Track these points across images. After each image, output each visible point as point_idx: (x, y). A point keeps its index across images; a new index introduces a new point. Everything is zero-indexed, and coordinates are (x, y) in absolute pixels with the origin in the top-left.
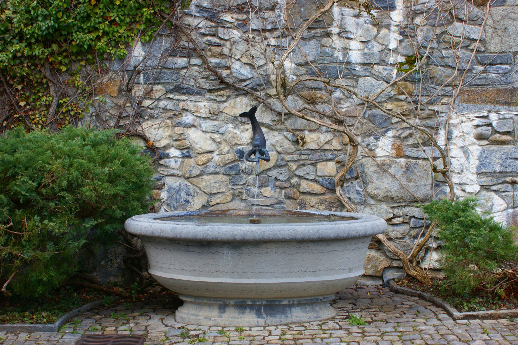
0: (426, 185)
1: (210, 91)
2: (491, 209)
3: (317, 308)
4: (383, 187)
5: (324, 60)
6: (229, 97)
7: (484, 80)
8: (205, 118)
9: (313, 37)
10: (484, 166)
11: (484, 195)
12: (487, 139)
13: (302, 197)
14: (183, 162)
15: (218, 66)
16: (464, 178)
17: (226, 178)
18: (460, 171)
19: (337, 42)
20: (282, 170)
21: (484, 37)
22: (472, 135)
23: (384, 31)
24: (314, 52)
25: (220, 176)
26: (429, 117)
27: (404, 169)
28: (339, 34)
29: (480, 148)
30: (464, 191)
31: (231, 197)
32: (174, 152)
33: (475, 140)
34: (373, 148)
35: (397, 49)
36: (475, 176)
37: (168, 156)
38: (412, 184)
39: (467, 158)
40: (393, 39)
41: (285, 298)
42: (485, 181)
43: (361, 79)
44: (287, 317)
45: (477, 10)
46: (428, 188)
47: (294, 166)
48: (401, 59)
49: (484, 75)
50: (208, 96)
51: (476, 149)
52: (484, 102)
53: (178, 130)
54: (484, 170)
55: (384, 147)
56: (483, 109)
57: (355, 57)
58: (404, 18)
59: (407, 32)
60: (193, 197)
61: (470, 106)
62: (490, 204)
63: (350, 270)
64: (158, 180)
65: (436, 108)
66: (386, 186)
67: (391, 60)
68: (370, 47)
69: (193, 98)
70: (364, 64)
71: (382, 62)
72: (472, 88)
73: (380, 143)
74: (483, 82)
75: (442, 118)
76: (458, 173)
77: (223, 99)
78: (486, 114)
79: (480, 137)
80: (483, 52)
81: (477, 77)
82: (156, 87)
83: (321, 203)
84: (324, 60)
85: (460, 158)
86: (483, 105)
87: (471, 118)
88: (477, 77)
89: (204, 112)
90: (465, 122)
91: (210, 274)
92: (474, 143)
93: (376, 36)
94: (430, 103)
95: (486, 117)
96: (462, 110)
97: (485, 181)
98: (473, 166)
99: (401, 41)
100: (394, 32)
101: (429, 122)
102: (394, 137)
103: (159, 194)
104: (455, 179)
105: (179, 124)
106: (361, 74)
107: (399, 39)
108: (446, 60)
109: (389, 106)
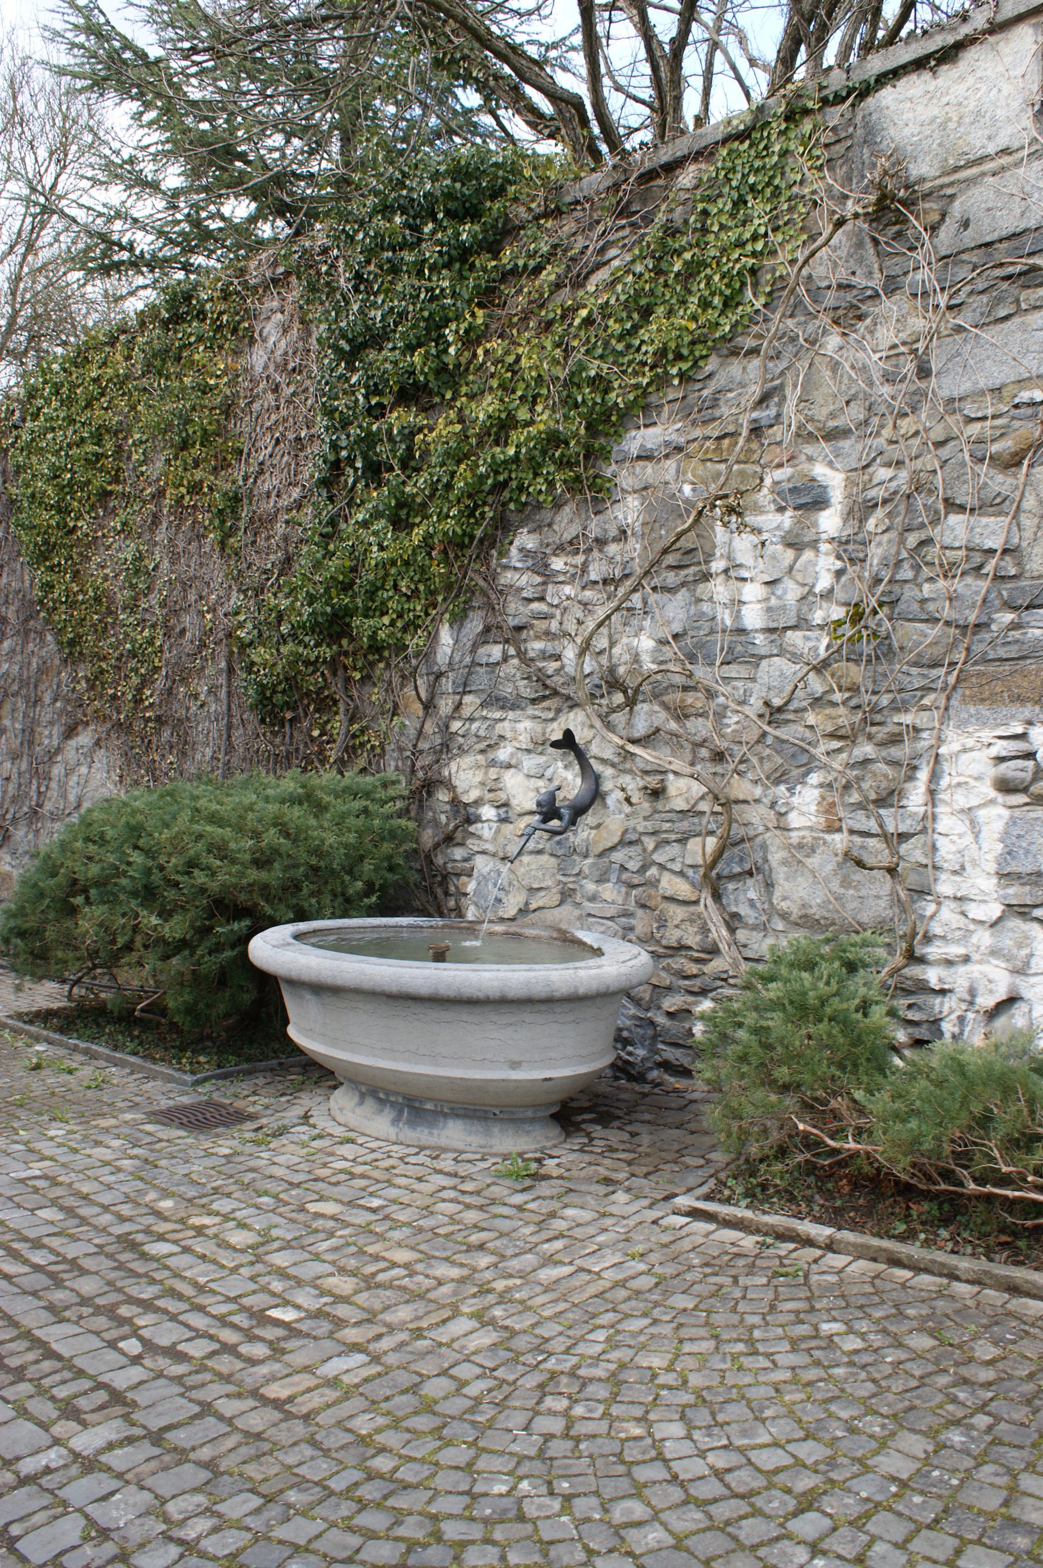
0: (878, 897)
1: (534, 701)
2: (1027, 964)
3: (496, 1130)
4: (795, 896)
5: (698, 628)
6: (558, 711)
7: (1016, 647)
8: (528, 751)
9: (683, 584)
10: (1013, 858)
11: (1012, 930)
12: (1025, 790)
13: (665, 905)
14: (498, 831)
15: (545, 656)
16: (964, 885)
17: (553, 861)
18: (957, 867)
19: (719, 589)
20: (633, 851)
21: (1016, 540)
22: (988, 782)
23: (808, 555)
24: (682, 615)
25: (545, 858)
26: (895, 739)
27: (840, 859)
28: (726, 571)
29: (1006, 813)
30: (964, 914)
31: (558, 897)
32: (488, 812)
33: (993, 793)
34: (783, 810)
35: (831, 591)
36: (994, 880)
37: (478, 819)
38: (851, 892)
39: (977, 836)
40: (823, 568)
41: (429, 1099)
42: (1016, 893)
43: (764, 663)
44: (431, 1134)
45: (1000, 478)
46: (883, 903)
47: (650, 843)
48: (838, 613)
49: (1016, 634)
50: (530, 711)
51: (996, 816)
52: (1019, 699)
53: (493, 773)
54: (1013, 867)
55: (805, 805)
56: (1013, 717)
57: (753, 617)
58: (845, 521)
59: (850, 549)
60: (507, 892)
61: (984, 710)
62: (1024, 952)
63: (515, 1065)
64: (466, 860)
65: (907, 719)
66: (803, 893)
67: (818, 617)
68: (779, 593)
69: (511, 715)
70: (771, 630)
71: (801, 624)
72: (991, 668)
73: (795, 800)
74: (1013, 652)
75: (927, 739)
76: (955, 872)
77: (551, 715)
78: (1019, 730)
79: (1005, 786)
80: (1014, 577)
81: (999, 641)
82: (468, 699)
83: (692, 921)
84: (698, 628)
85: (960, 836)
86: (1014, 709)
87: (986, 741)
88: (999, 641)
89: (524, 741)
90: (971, 750)
91: (334, 1043)
92: (992, 802)
93: (791, 568)
94: (896, 707)
95: (1023, 737)
96: (965, 723)
97: (1016, 893)
98: (989, 857)
99: (839, 573)
100: (827, 554)
101: (895, 752)
102: (821, 785)
103: (465, 885)
104: (945, 886)
105: (493, 763)
106: (763, 652)
107: (834, 568)
108: (931, 607)
109: (811, 718)
